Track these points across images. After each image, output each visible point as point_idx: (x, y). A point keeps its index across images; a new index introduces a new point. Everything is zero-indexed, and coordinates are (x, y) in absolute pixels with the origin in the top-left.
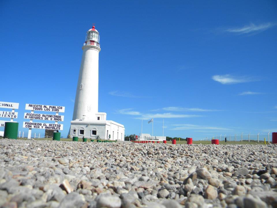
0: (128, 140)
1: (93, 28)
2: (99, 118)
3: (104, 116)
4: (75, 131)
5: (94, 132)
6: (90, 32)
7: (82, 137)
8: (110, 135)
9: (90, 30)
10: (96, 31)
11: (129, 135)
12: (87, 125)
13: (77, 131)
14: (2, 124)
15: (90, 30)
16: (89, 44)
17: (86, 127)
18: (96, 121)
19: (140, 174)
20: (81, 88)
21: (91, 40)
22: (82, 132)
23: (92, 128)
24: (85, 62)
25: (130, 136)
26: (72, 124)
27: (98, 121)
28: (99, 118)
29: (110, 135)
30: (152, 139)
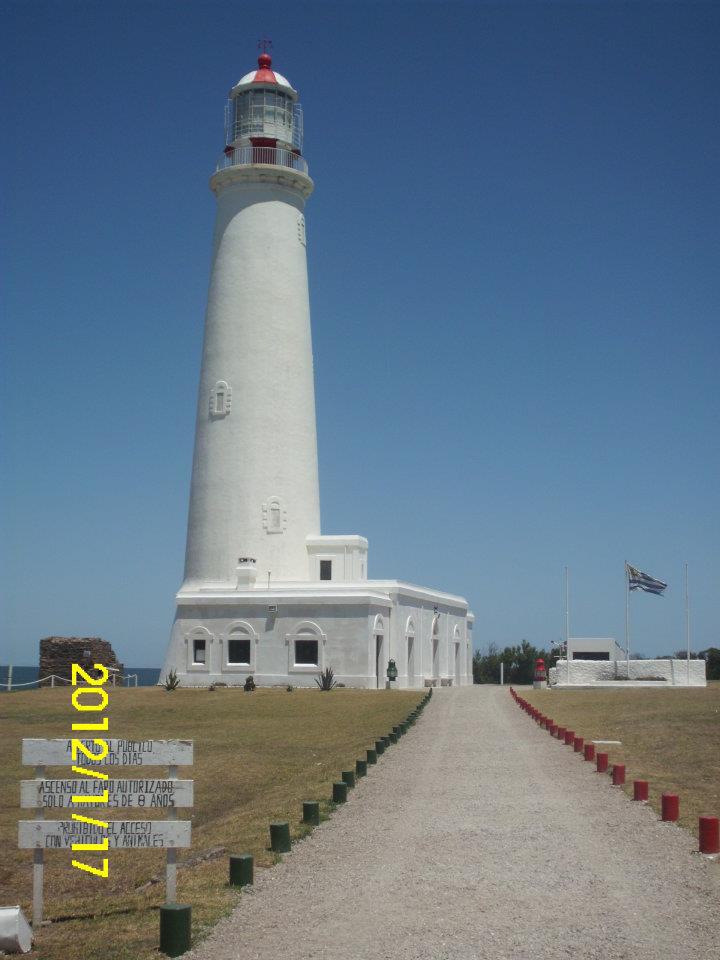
0: (496, 681)
1: (264, 65)
2: (326, 571)
3: (350, 551)
4: (200, 645)
5: (307, 651)
6: (246, 91)
7: (242, 680)
8: (392, 665)
9: (249, 78)
10: (281, 80)
11: (508, 639)
12: (270, 612)
13: (210, 648)
14: (631, 588)
15: (249, 78)
16: (243, 162)
17: (269, 627)
18: (311, 588)
19: (542, 742)
20: (221, 403)
21: (256, 135)
22: (240, 651)
23: (294, 629)
24: (223, 243)
25: (507, 650)
26: (186, 611)
27: (326, 584)
28: (326, 571)
29: (392, 665)
30: (627, 679)
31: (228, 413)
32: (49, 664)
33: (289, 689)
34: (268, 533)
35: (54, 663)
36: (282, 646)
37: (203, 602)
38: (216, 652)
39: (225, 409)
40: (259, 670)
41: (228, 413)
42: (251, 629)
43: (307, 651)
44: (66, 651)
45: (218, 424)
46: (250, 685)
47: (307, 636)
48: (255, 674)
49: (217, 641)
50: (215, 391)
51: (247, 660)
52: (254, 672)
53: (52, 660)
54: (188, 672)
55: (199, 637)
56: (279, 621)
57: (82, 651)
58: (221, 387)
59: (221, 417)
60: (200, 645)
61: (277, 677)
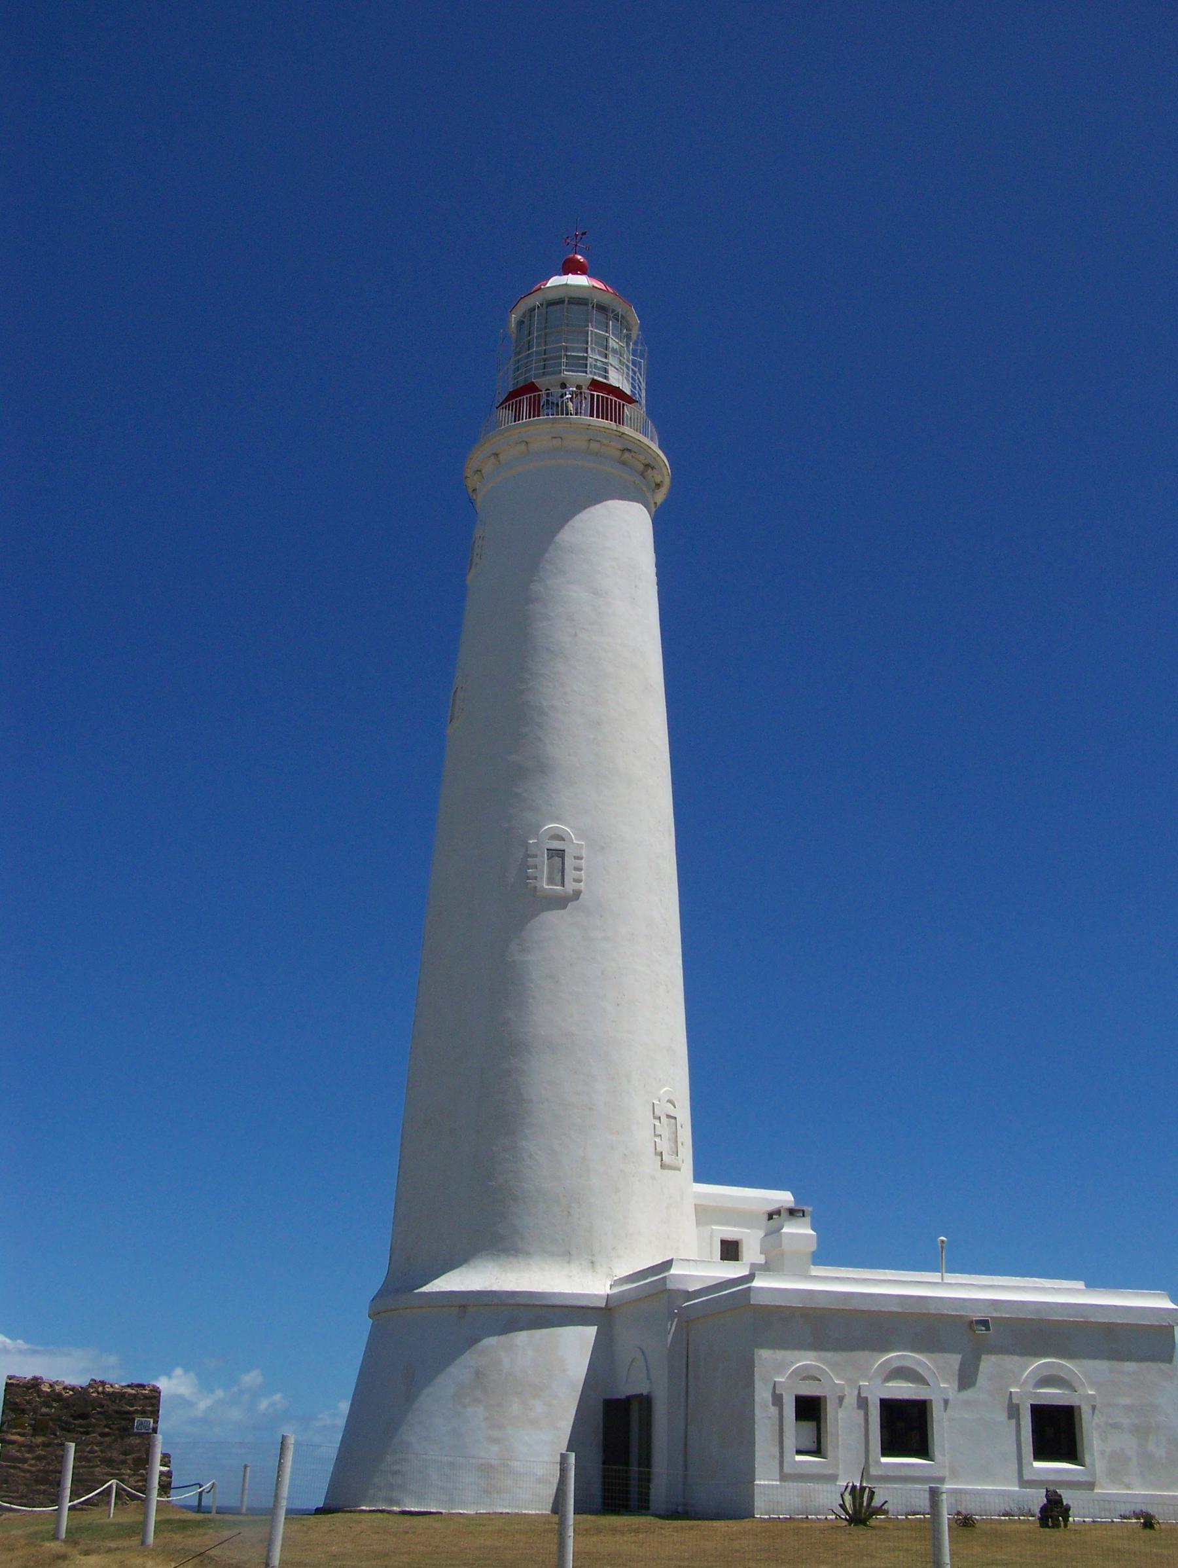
5: (1056, 1432)
17: (966, 1379)
20: (560, 874)
22: (906, 1427)
23: (1027, 1379)
31: (577, 894)
32: (31, 1448)
33: (1149, 1523)
34: (663, 1166)
35: (45, 1445)
36: (1002, 1416)
37: (824, 1303)
38: (852, 1430)
39: (570, 886)
40: (955, 1475)
41: (577, 894)
42: (933, 1378)
43: (1056, 1432)
44: (83, 1416)
45: (552, 917)
46: (1054, 1511)
47: (1053, 1395)
48: (947, 1486)
49: (851, 1400)
50: (540, 843)
51: (923, 1450)
52: (942, 1480)
53: (40, 1439)
54: (783, 1477)
55: (808, 1390)
56: (988, 1364)
57: (128, 1417)
58: (560, 838)
59: (561, 902)
60: (810, 1409)
61: (1000, 1493)
